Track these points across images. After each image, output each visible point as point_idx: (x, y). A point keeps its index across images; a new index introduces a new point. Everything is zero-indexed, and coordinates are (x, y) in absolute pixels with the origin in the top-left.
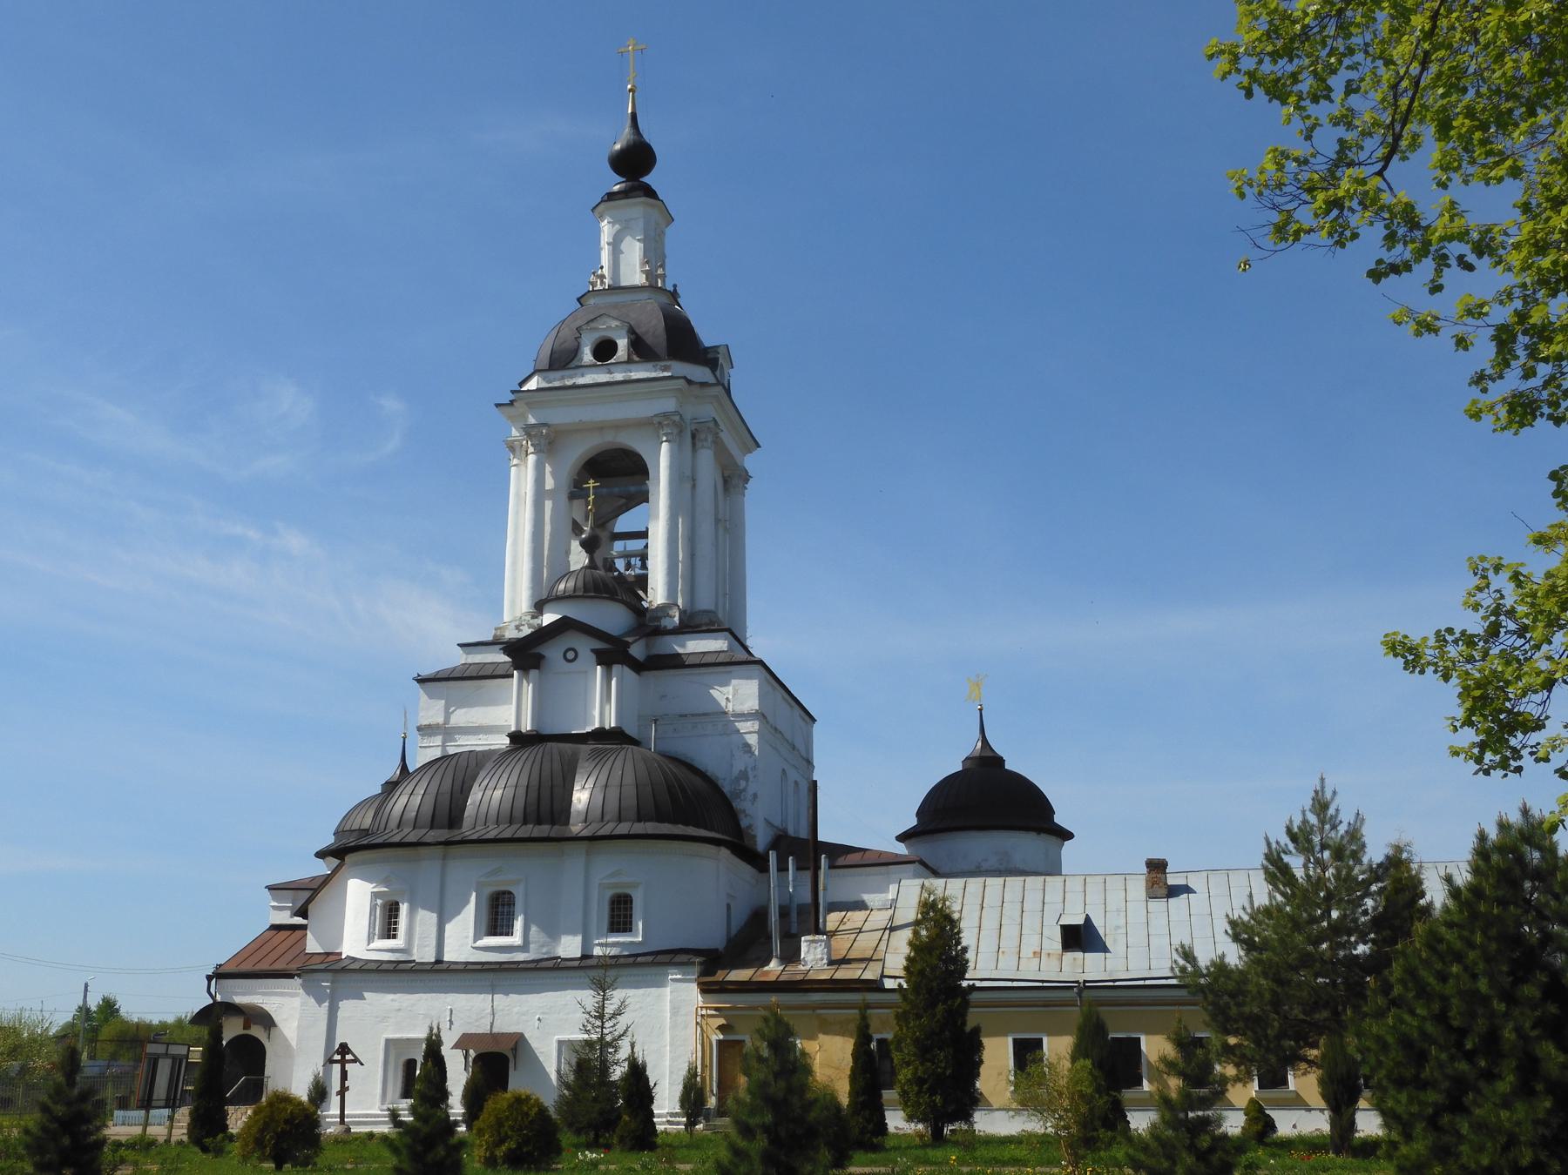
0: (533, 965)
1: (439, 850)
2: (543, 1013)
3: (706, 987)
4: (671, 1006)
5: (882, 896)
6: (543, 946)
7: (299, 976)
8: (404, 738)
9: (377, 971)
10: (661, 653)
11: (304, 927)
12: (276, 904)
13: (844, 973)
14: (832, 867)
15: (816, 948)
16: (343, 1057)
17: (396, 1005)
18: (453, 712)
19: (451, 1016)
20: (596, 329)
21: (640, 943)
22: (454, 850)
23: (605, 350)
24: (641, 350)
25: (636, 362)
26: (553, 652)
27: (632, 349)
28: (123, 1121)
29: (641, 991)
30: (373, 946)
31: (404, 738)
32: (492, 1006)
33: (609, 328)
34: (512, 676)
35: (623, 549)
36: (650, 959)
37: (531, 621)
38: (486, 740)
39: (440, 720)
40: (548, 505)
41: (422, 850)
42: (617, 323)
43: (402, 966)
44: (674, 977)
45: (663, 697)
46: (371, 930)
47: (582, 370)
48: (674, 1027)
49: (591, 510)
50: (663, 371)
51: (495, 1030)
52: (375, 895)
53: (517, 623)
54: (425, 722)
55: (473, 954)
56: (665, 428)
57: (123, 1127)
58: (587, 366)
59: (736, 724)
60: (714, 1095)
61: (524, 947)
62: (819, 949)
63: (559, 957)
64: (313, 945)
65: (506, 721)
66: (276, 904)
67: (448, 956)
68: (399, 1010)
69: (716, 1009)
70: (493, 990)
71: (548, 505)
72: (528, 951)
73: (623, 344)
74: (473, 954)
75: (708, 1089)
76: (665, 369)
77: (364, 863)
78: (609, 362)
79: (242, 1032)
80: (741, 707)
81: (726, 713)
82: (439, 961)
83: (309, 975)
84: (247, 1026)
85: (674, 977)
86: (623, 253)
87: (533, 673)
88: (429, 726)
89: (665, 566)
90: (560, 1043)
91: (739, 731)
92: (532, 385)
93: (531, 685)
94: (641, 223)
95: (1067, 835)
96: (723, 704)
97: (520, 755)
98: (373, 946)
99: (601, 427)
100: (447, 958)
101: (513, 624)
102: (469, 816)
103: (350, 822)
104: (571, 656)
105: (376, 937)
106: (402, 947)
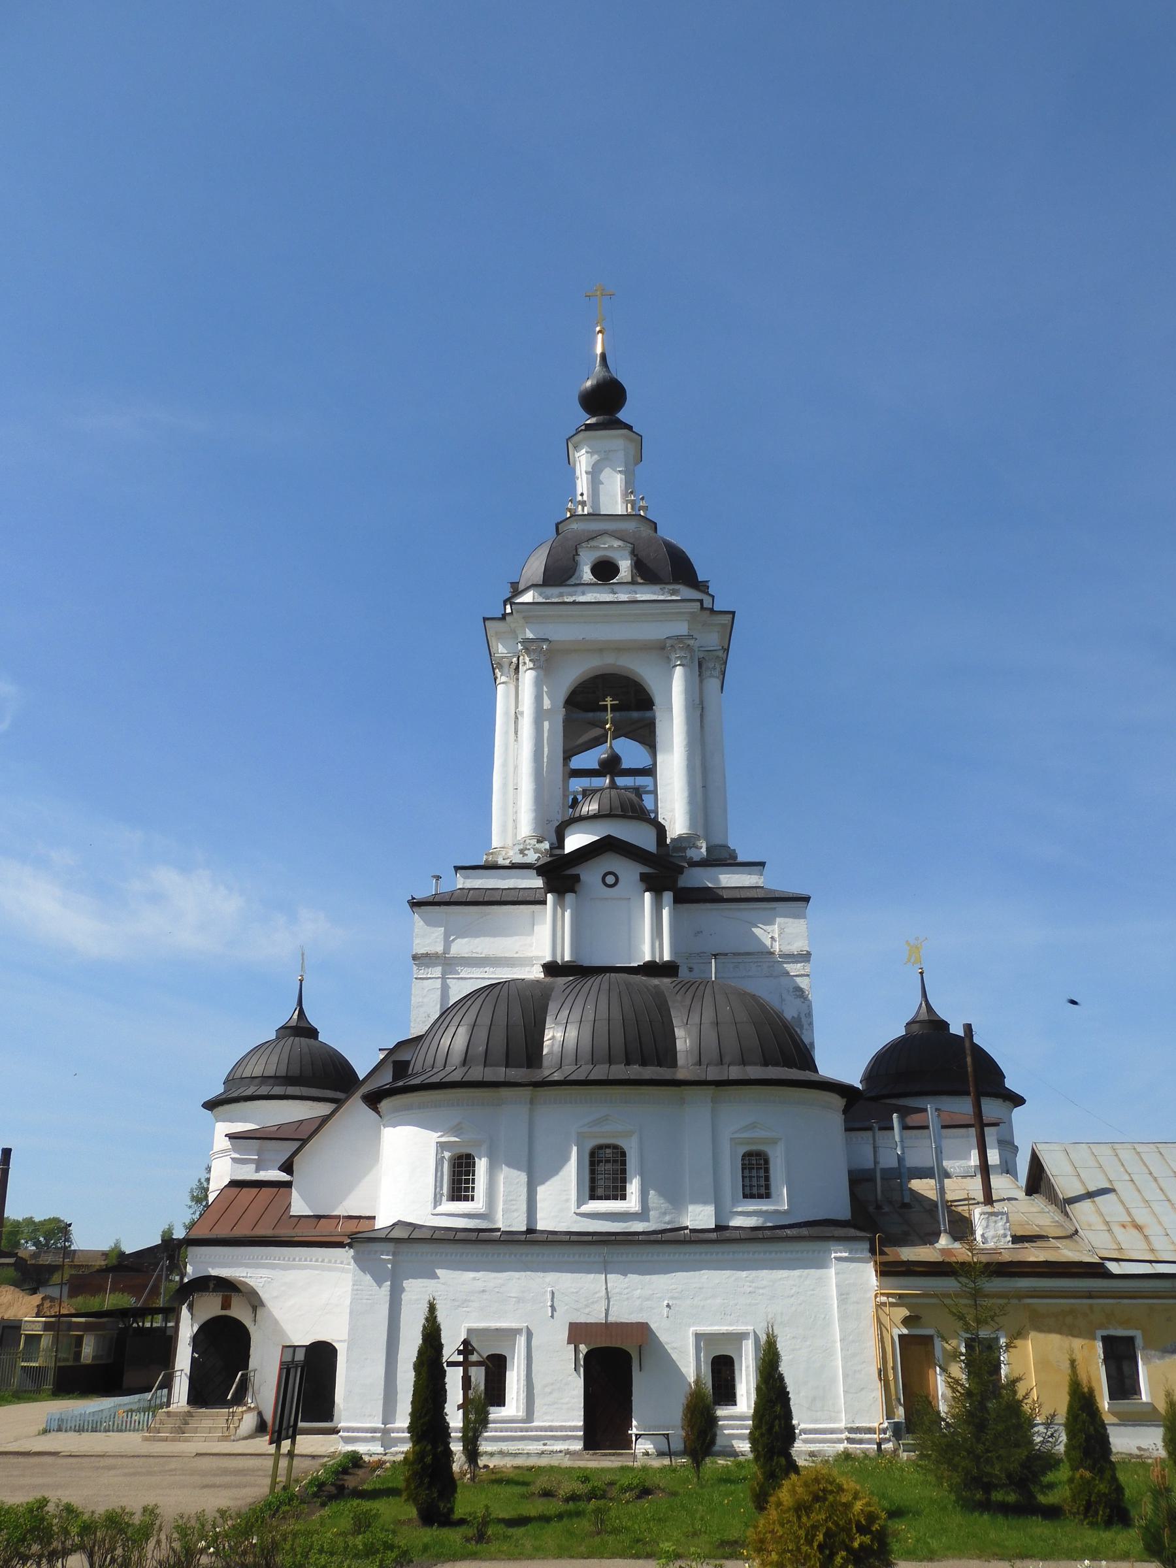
0: (473, 1236)
1: (526, 1092)
2: (672, 1298)
3: (886, 1269)
4: (837, 1292)
5: (963, 1163)
6: (665, 1214)
7: (350, 1245)
8: (301, 981)
9: (432, 1240)
10: (689, 886)
11: (288, 1185)
12: (237, 1156)
13: (1034, 1254)
14: (905, 1127)
15: (996, 1222)
16: (465, 1358)
17: (479, 1285)
18: (453, 940)
19: (552, 1300)
20: (597, 548)
21: (785, 1212)
22: (543, 1092)
23: (605, 571)
24: (645, 572)
25: (640, 583)
26: (590, 875)
27: (635, 571)
28: (59, 1426)
29: (797, 1273)
30: (440, 1209)
31: (301, 981)
32: (606, 1289)
33: (611, 547)
34: (544, 902)
35: (589, 786)
36: (804, 1231)
37: (538, 846)
38: (493, 973)
39: (439, 949)
40: (546, 724)
41: (505, 1092)
42: (620, 543)
43: (483, 1235)
44: (839, 1255)
45: (698, 933)
46: (438, 1189)
47: (580, 589)
48: (843, 1317)
49: (610, 729)
50: (672, 595)
51: (611, 1319)
52: (442, 1146)
53: (521, 847)
54: (422, 951)
55: (576, 1222)
56: (678, 651)
57: (61, 1435)
58: (587, 584)
59: (785, 965)
60: (901, 1405)
61: (643, 1215)
62: (1000, 1224)
63: (686, 1228)
64: (299, 1206)
65: (517, 953)
66: (237, 1156)
67: (544, 1223)
68: (484, 1291)
69: (900, 1296)
70: (606, 1268)
71: (546, 724)
72: (648, 1221)
73: (625, 566)
74: (576, 1222)
75: (894, 1397)
76: (674, 593)
77: (409, 1108)
78: (611, 582)
79: (219, 1312)
80: (789, 947)
81: (773, 953)
82: (530, 1231)
83: (366, 1245)
84: (226, 1305)
85: (839, 1255)
86: (603, 484)
87: (569, 897)
88: (427, 955)
89: (686, 794)
90: (698, 1336)
91: (788, 973)
92: (528, 597)
93: (567, 914)
94: (621, 454)
95: (1018, 1101)
96: (768, 942)
97: (584, 982)
98: (440, 1209)
99: (601, 648)
100: (540, 1226)
101: (517, 848)
102: (550, 1053)
103: (241, 1069)
104: (611, 881)
105: (444, 1198)
106: (482, 1211)
